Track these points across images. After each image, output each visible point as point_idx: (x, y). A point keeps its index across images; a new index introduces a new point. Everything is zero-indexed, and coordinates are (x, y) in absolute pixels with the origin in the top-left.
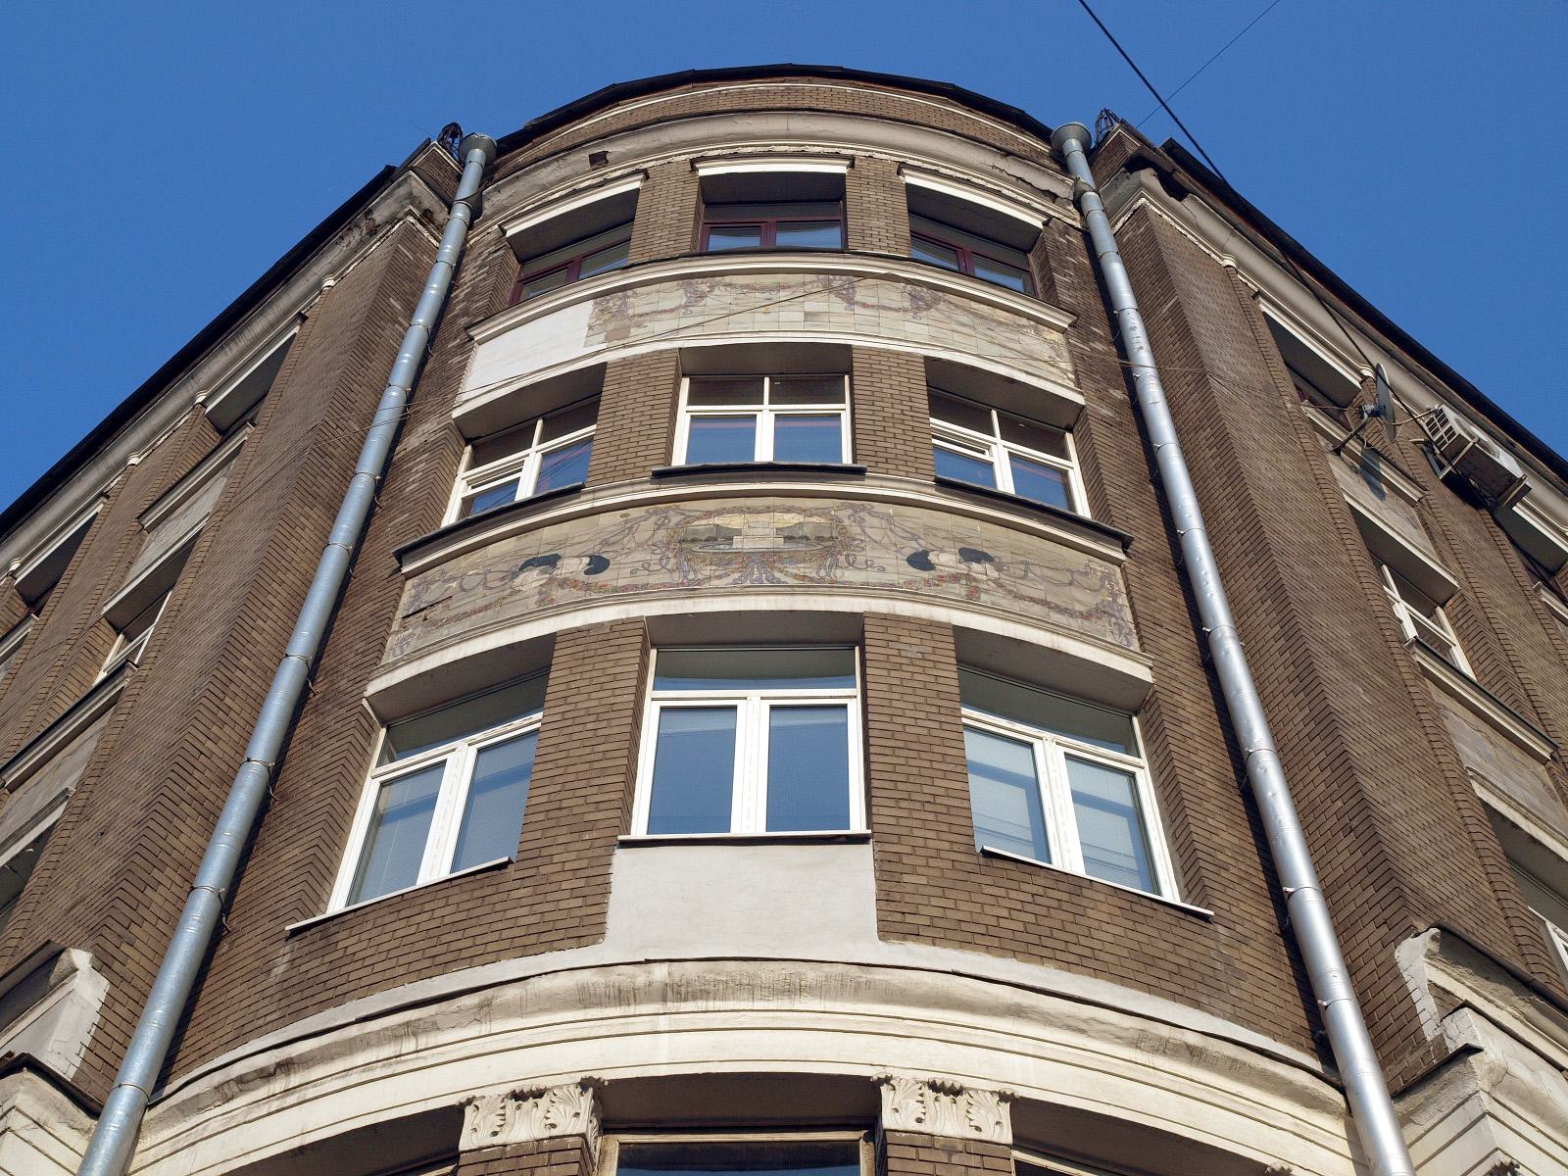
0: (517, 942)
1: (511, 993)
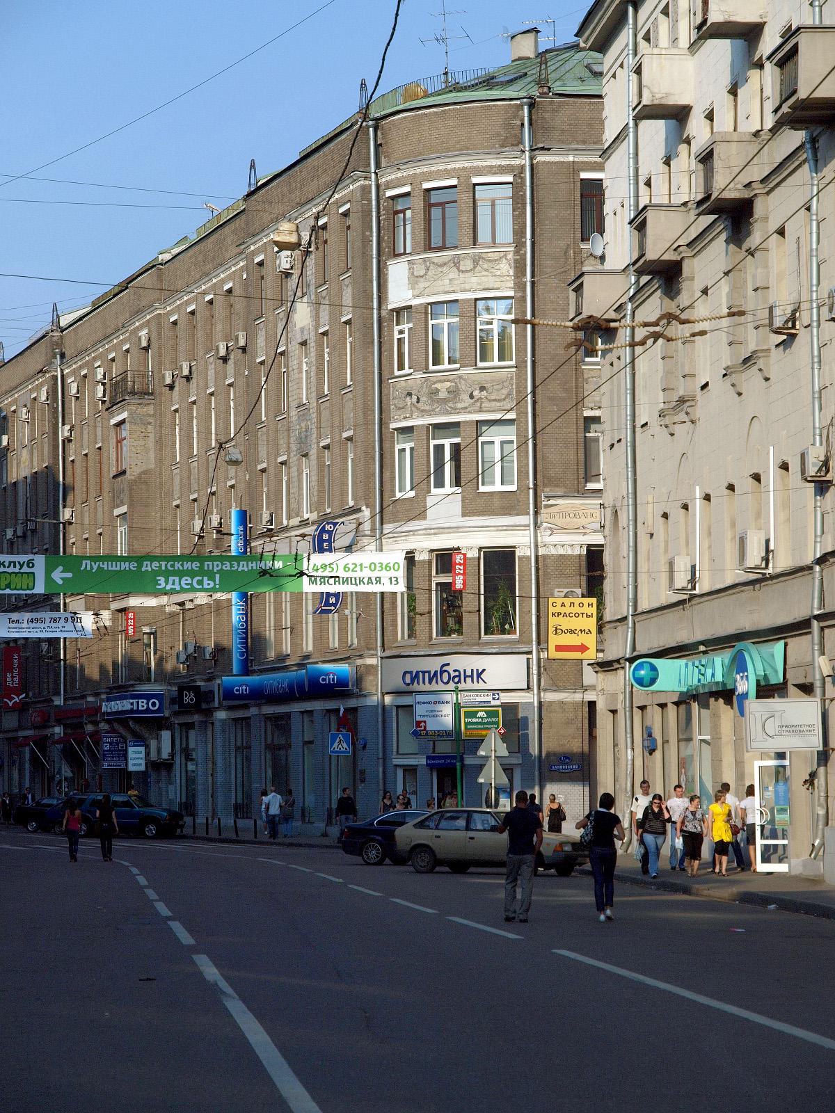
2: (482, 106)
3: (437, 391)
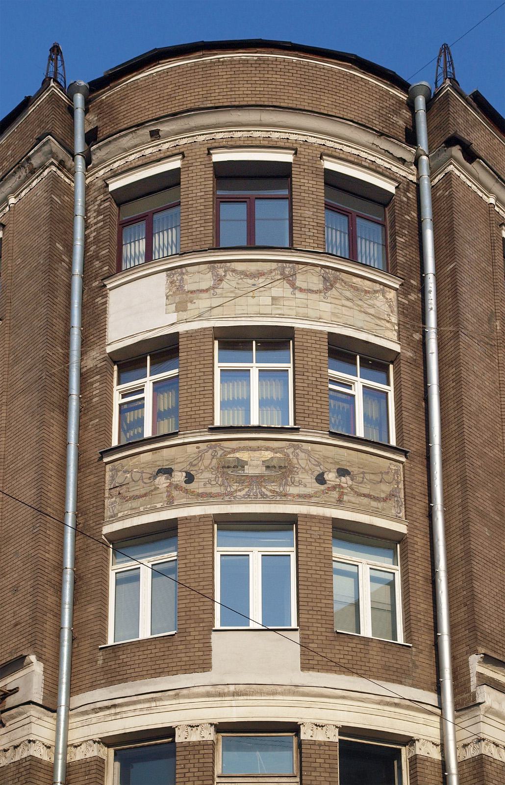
0: (183, 667)
1: (185, 692)
2: (340, 72)
3: (241, 464)
